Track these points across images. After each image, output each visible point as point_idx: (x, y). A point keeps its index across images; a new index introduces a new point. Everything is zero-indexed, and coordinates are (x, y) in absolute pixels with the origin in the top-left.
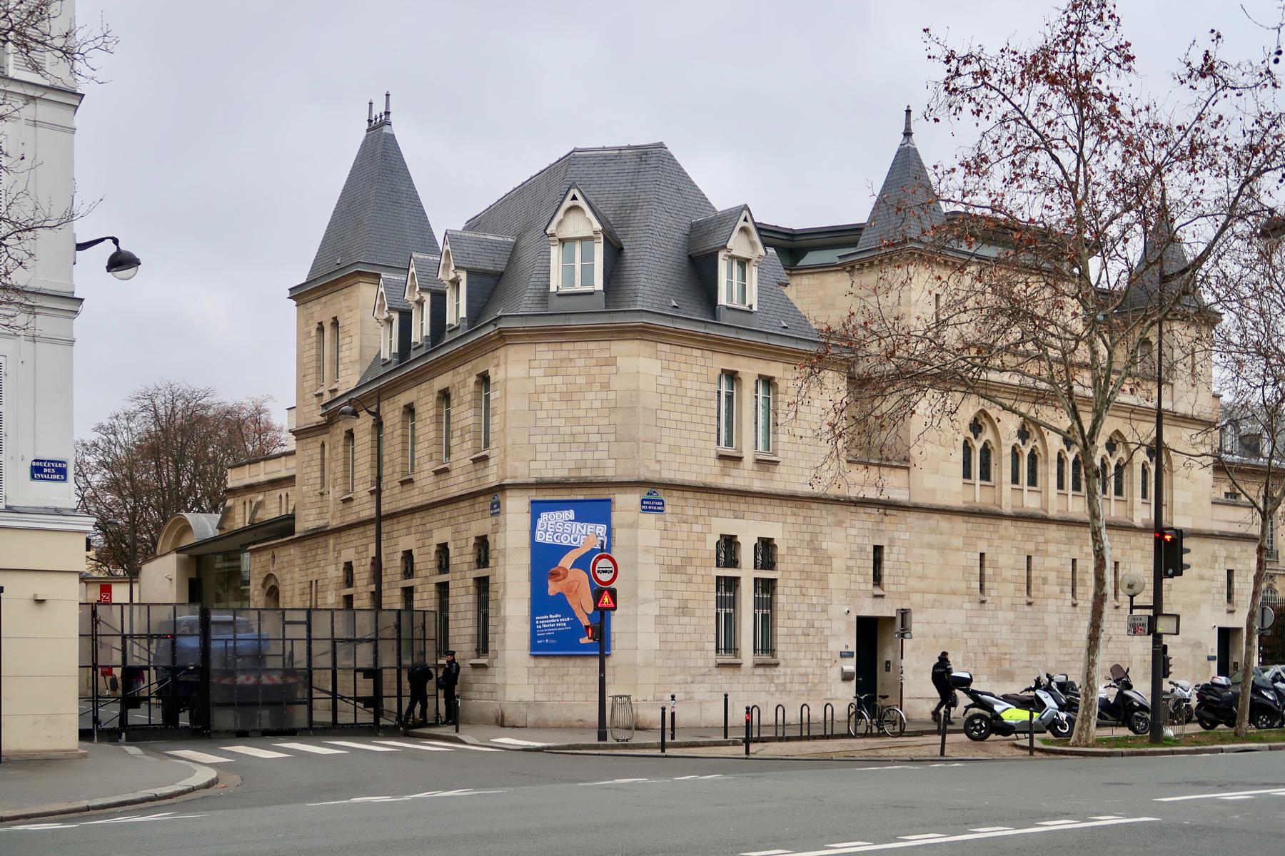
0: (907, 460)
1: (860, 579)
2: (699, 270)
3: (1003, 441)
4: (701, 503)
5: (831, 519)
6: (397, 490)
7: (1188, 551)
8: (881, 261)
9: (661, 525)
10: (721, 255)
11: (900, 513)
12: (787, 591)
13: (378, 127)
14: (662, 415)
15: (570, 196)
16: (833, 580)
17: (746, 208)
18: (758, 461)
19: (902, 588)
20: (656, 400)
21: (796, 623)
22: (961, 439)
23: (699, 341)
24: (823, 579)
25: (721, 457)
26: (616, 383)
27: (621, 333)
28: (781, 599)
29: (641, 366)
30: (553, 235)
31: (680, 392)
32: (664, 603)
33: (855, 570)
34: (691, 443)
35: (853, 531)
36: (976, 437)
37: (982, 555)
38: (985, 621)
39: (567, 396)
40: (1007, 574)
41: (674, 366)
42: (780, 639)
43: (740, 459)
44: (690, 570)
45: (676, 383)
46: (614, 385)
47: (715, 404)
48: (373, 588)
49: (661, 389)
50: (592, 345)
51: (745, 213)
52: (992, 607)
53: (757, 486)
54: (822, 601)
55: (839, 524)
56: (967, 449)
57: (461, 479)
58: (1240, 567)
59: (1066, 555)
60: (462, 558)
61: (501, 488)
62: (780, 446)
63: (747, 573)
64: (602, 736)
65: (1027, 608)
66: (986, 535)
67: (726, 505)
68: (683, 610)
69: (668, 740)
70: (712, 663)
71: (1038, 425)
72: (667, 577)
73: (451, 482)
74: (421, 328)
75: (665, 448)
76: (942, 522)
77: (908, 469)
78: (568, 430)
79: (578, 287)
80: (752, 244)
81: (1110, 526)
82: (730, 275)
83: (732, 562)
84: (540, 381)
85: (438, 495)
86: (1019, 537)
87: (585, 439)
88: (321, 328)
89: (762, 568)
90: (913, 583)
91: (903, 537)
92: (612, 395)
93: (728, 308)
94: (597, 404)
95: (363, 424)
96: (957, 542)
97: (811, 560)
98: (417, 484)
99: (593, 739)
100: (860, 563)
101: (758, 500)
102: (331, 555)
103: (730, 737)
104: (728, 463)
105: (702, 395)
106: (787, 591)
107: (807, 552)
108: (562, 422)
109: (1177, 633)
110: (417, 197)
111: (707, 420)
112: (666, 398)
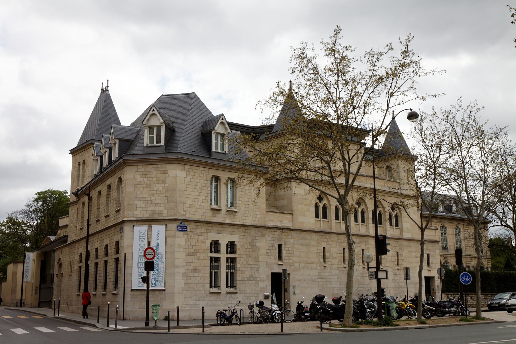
0: (292, 211)
1: (272, 257)
2: (205, 138)
3: (331, 203)
4: (203, 228)
5: (259, 234)
6: (95, 224)
7: (389, 244)
8: (281, 136)
9: (186, 236)
10: (213, 132)
11: (289, 232)
12: (241, 262)
13: (105, 92)
14: (187, 193)
15: (152, 110)
16: (261, 258)
17: (222, 115)
18: (228, 211)
19: (291, 261)
20: (187, 187)
21: (245, 276)
22: (314, 203)
23: (202, 164)
24: (256, 258)
25: (212, 209)
26: (168, 180)
27: (171, 161)
28: (238, 266)
29: (178, 174)
30: (145, 124)
31: (194, 183)
32: (187, 267)
33: (270, 254)
34: (199, 204)
35: (269, 239)
36: (320, 202)
37: (324, 248)
38: (327, 274)
39: (149, 186)
40: (335, 255)
41: (191, 173)
42: (238, 282)
43: (220, 210)
44: (198, 254)
45: (193, 180)
46: (167, 181)
47: (209, 189)
48: (89, 263)
49: (186, 183)
50: (159, 166)
51: (222, 117)
52: (329, 268)
53: (228, 221)
54: (256, 266)
55: (263, 236)
56: (317, 207)
57: (112, 219)
58: (432, 253)
59: (359, 248)
60: (112, 250)
61: (123, 222)
62: (237, 205)
63: (223, 255)
64: (147, 324)
65: (397, 271)
66: (326, 240)
67: (214, 228)
68: (195, 270)
69: (242, 322)
70: (208, 292)
71: (325, 194)
72: (188, 257)
73: (110, 220)
74: (106, 162)
75: (188, 206)
76: (307, 235)
77: (292, 214)
78: (149, 199)
79: (155, 144)
80: (226, 128)
81: (438, 242)
82: (217, 139)
83: (217, 251)
84: (139, 180)
85: (106, 226)
86: (339, 241)
87: (155, 202)
88: (79, 165)
89: (231, 253)
90: (295, 259)
91: (291, 242)
92: (166, 185)
93: (216, 152)
94: (161, 189)
95: (86, 199)
96: (313, 243)
97: (251, 250)
98: (101, 221)
99: (143, 325)
100: (272, 251)
101: (228, 226)
102: (77, 250)
103: (180, 325)
104: (215, 211)
105: (204, 185)
106: (241, 262)
107: (249, 247)
108: (147, 196)
109: (387, 278)
110: (117, 117)
111: (206, 195)
112: (188, 186)
